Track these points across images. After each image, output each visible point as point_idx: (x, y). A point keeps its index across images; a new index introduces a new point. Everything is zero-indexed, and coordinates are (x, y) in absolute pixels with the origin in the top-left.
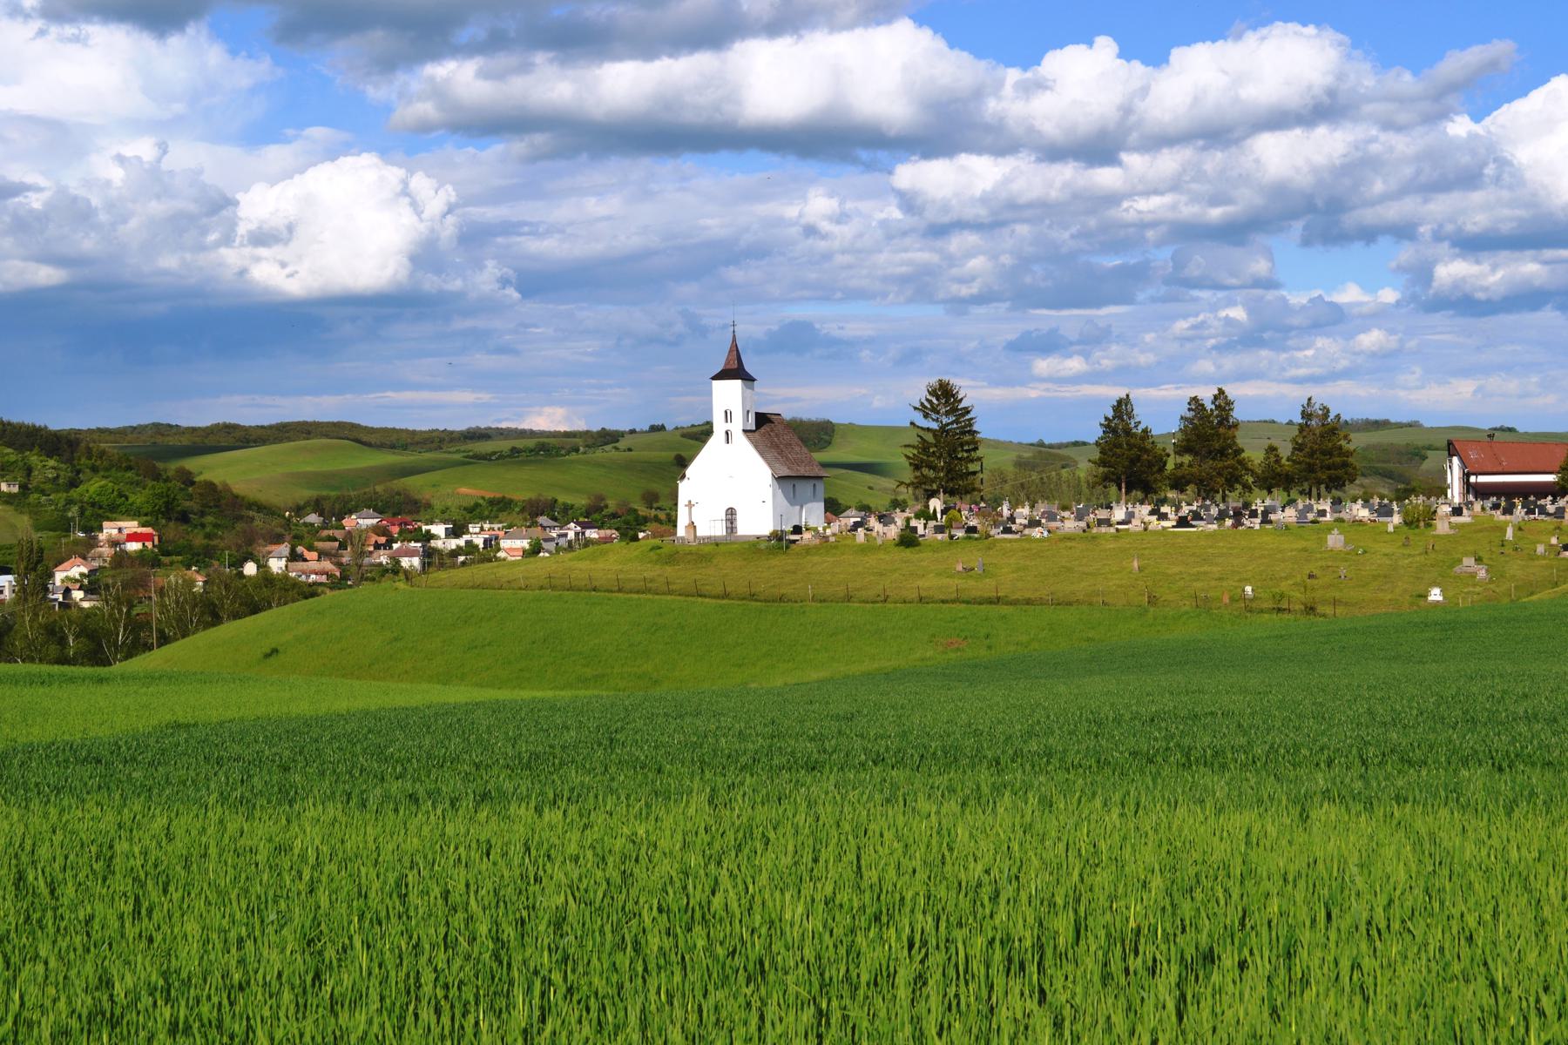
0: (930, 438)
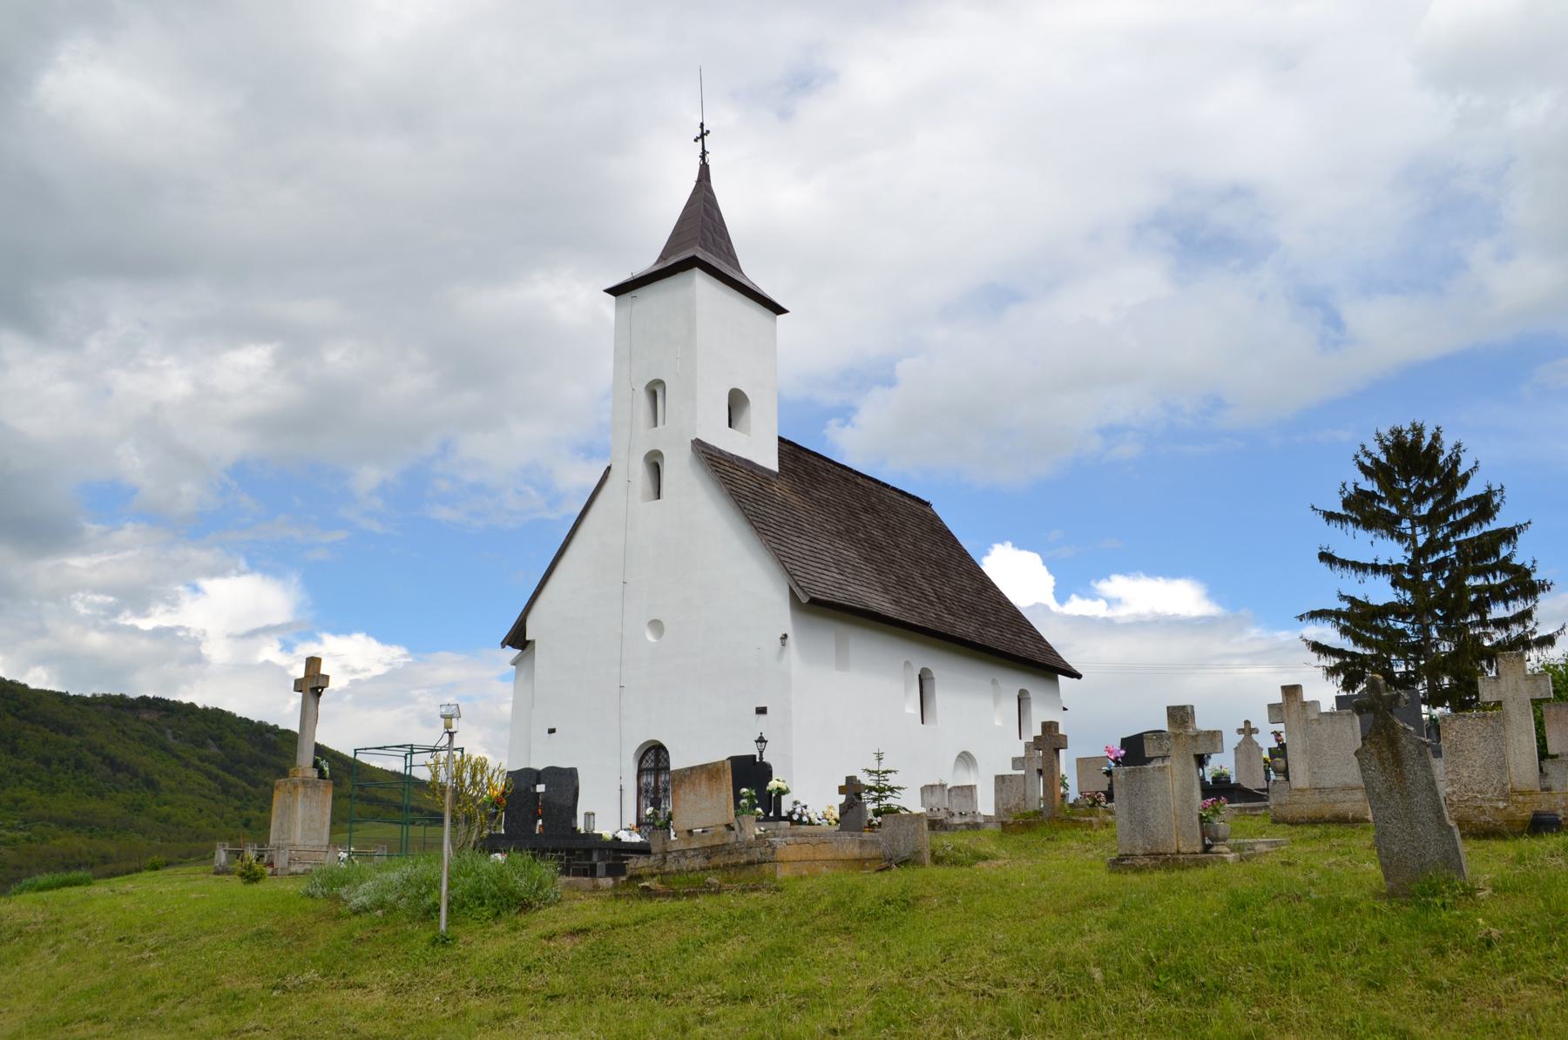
0: (1380, 592)
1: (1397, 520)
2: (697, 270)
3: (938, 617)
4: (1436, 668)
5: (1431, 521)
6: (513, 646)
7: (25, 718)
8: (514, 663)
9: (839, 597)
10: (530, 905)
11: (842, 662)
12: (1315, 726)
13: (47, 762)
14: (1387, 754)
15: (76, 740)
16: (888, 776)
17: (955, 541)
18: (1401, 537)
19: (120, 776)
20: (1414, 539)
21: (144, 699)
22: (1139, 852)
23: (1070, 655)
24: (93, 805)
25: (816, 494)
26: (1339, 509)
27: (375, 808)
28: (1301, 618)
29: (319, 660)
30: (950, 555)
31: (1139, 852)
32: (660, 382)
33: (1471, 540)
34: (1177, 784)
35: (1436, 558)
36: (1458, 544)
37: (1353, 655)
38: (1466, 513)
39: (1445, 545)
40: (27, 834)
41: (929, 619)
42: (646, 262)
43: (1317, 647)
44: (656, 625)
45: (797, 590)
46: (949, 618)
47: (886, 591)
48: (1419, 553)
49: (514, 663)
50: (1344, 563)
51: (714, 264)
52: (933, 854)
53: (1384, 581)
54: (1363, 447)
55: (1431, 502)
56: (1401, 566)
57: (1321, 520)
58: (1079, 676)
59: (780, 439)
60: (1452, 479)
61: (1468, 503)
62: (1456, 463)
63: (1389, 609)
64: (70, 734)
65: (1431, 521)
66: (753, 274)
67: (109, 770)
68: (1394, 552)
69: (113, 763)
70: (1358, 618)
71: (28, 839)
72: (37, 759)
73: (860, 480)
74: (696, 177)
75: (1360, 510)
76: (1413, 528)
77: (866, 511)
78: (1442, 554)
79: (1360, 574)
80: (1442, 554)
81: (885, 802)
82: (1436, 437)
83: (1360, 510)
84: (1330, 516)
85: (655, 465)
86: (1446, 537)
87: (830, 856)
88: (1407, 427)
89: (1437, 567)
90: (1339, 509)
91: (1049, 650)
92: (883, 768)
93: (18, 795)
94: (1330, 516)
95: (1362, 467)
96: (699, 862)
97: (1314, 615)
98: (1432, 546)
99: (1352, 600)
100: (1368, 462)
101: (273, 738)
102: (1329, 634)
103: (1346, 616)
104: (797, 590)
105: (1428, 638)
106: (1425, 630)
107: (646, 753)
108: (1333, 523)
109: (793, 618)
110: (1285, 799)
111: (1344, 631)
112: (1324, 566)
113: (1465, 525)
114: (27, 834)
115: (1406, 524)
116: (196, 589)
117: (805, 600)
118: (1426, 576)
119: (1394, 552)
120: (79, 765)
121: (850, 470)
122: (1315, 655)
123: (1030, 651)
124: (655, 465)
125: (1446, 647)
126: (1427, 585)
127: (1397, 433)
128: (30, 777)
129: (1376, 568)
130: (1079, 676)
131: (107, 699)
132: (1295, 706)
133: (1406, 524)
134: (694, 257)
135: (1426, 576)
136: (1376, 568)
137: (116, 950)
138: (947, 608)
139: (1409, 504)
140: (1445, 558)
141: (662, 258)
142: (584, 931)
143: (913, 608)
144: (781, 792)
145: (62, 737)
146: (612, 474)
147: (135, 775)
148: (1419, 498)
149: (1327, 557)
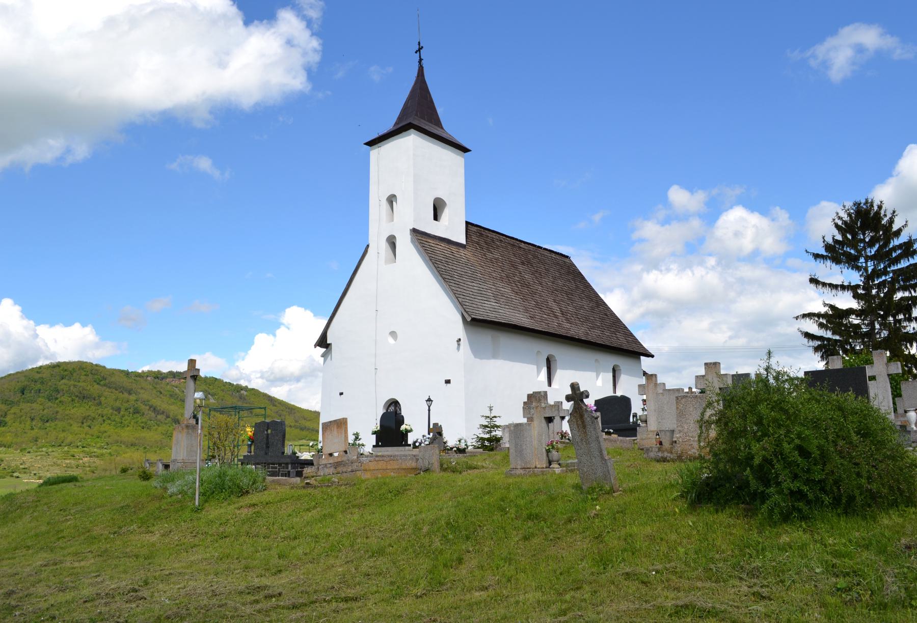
0: (846, 302)
1: (856, 259)
2: (412, 130)
3: (559, 325)
4: (878, 346)
5: (876, 257)
6: (321, 346)
7: (105, 385)
8: (322, 356)
9: (492, 317)
10: (247, 492)
11: (495, 356)
12: (661, 396)
13: (119, 410)
14: (580, 422)
15: (133, 397)
16: (495, 419)
17: (583, 278)
18: (858, 268)
19: (159, 417)
20: (866, 269)
21: (171, 373)
22: (519, 467)
23: (647, 345)
24: (146, 434)
25: (489, 255)
26: (823, 252)
27: (304, 433)
28: (797, 318)
29: (195, 361)
30: (577, 287)
31: (519, 467)
32: (394, 196)
33: (902, 269)
34: (536, 432)
35: (881, 280)
36: (894, 272)
37: (829, 339)
38: (899, 252)
39: (885, 273)
40: (108, 451)
41: (553, 326)
42: (389, 125)
43: (808, 335)
44: (393, 334)
45: (465, 314)
46: (567, 325)
47: (526, 311)
48: (869, 278)
49: (322, 356)
50: (824, 284)
51: (426, 128)
52: (441, 465)
53: (849, 294)
54: (837, 214)
55: (877, 246)
56: (858, 286)
57: (811, 258)
58: (652, 356)
59: (467, 223)
60: (889, 233)
61: (900, 246)
62: (891, 221)
63: (850, 311)
64: (130, 394)
65: (876, 257)
66: (450, 128)
67: (153, 415)
68: (855, 278)
69: (155, 409)
70: (835, 317)
71: (110, 453)
72: (113, 409)
73: (523, 245)
74: (416, 74)
75: (834, 253)
76: (866, 262)
77: (523, 263)
78: (884, 278)
79: (834, 291)
80: (884, 278)
81: (494, 433)
82: (880, 207)
83: (834, 253)
84: (817, 256)
85: (392, 242)
86: (885, 268)
87: (396, 467)
88: (863, 201)
89: (880, 286)
90: (823, 252)
91: (636, 341)
92: (493, 415)
93: (102, 429)
94: (817, 256)
95: (837, 226)
96: (332, 470)
97: (804, 316)
98: (876, 273)
99: (832, 307)
100: (840, 223)
101: (245, 393)
102: (812, 327)
103: (825, 316)
104: (465, 314)
105: (873, 328)
106: (872, 324)
107: (389, 406)
108: (818, 260)
109: (465, 329)
110: (644, 436)
111: (821, 325)
112: (813, 286)
113: (897, 260)
114: (108, 451)
115: (862, 260)
116: (642, 240)
117: (469, 319)
118: (874, 292)
119: (855, 278)
120: (136, 411)
121: (517, 239)
122: (806, 340)
123: (622, 342)
124: (392, 242)
125: (885, 333)
126: (874, 297)
127: (857, 204)
128: (109, 418)
129: (843, 287)
130: (652, 356)
131: (150, 373)
132: (652, 385)
133: (862, 260)
134: (410, 123)
135: (874, 292)
136: (843, 287)
137: (58, 514)
138: (567, 319)
139: (864, 248)
140: (886, 280)
141: (396, 124)
142: (254, 505)
143: (542, 320)
144: (407, 431)
145: (126, 395)
146: (370, 250)
147: (168, 417)
148: (871, 244)
149: (814, 281)
